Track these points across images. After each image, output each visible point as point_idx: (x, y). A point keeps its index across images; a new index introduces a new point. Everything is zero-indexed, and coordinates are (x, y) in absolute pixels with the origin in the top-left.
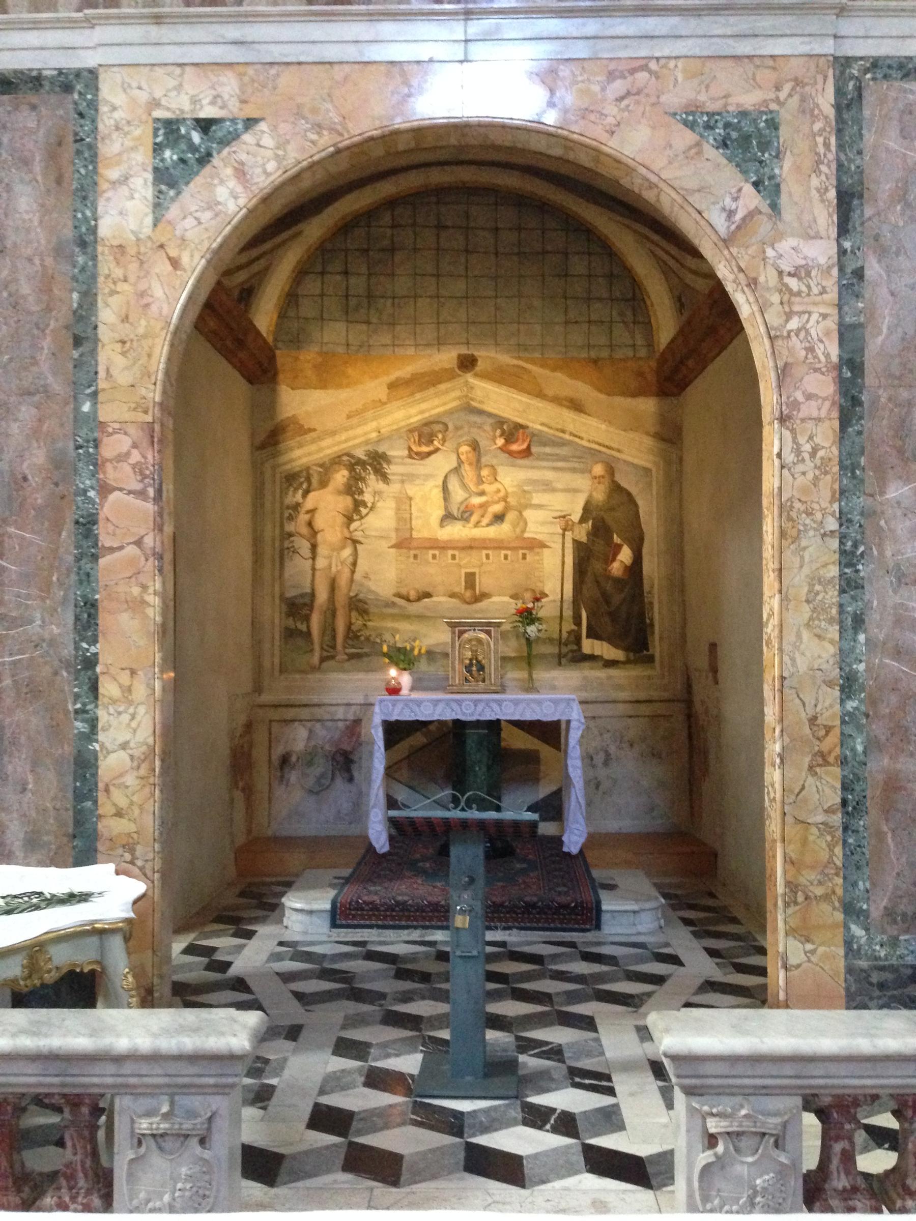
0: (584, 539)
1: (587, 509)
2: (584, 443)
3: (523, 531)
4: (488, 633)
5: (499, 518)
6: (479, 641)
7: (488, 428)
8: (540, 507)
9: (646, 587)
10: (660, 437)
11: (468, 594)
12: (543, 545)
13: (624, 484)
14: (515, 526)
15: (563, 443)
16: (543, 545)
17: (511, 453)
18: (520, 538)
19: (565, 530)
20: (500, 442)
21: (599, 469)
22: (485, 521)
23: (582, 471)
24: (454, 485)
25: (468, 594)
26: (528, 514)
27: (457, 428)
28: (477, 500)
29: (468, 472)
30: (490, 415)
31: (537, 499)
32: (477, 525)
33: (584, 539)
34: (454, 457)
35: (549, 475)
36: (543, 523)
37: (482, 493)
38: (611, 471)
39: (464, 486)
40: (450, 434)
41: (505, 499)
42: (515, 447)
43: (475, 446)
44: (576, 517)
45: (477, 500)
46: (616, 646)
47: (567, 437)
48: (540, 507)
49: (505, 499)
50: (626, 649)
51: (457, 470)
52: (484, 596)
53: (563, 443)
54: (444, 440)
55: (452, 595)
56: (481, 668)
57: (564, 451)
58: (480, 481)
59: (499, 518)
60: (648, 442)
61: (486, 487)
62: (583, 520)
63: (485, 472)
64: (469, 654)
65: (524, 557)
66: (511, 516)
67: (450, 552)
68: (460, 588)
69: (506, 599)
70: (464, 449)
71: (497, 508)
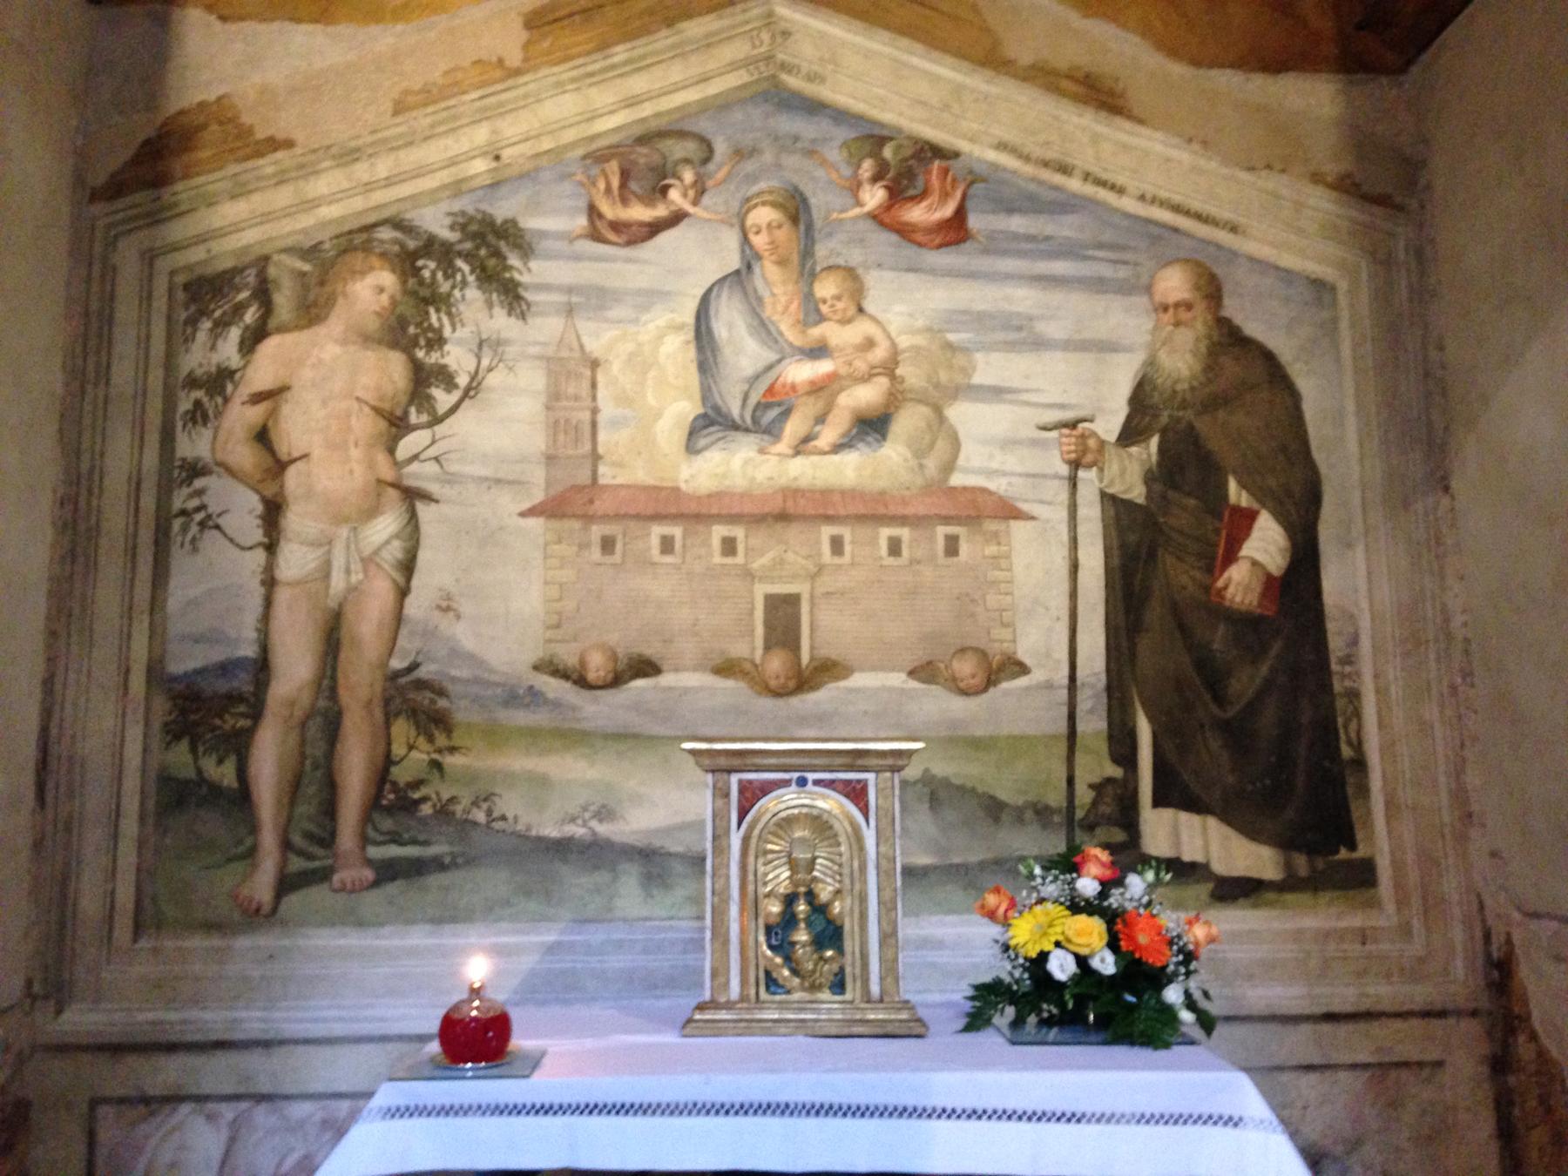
0: (1137, 493)
1: (1141, 399)
2: (1128, 204)
3: (949, 467)
4: (856, 793)
5: (872, 426)
6: (820, 824)
7: (834, 154)
8: (996, 393)
9: (1336, 644)
10: (1347, 186)
11: (776, 665)
12: (1010, 512)
13: (1253, 328)
14: (920, 453)
15: (1064, 205)
16: (1010, 512)
17: (905, 232)
18: (939, 488)
19: (1076, 465)
20: (874, 197)
21: (1174, 283)
22: (829, 435)
23: (1124, 289)
24: (730, 321)
25: (776, 665)
26: (960, 413)
27: (740, 154)
28: (801, 372)
29: (774, 283)
30: (841, 116)
31: (989, 368)
32: (803, 445)
33: (1137, 493)
34: (731, 240)
35: (1022, 299)
36: (1008, 444)
37: (818, 351)
38: (1211, 289)
39: (763, 328)
40: (719, 167)
41: (889, 368)
42: (917, 214)
43: (796, 208)
44: (1109, 425)
45: (801, 372)
46: (1252, 833)
47: (1075, 184)
48: (996, 393)
49: (889, 368)
50: (1286, 843)
51: (739, 278)
52: (827, 670)
53: (1064, 205)
54: (700, 189)
55: (727, 668)
56: (829, 934)
57: (1065, 228)
58: (812, 312)
59: (872, 426)
60: (1321, 203)
61: (831, 332)
62: (1130, 434)
63: (826, 288)
64: (780, 878)
65: (952, 547)
66: (907, 422)
67: (719, 531)
68: (751, 645)
69: (898, 679)
70: (763, 215)
71: (867, 395)
